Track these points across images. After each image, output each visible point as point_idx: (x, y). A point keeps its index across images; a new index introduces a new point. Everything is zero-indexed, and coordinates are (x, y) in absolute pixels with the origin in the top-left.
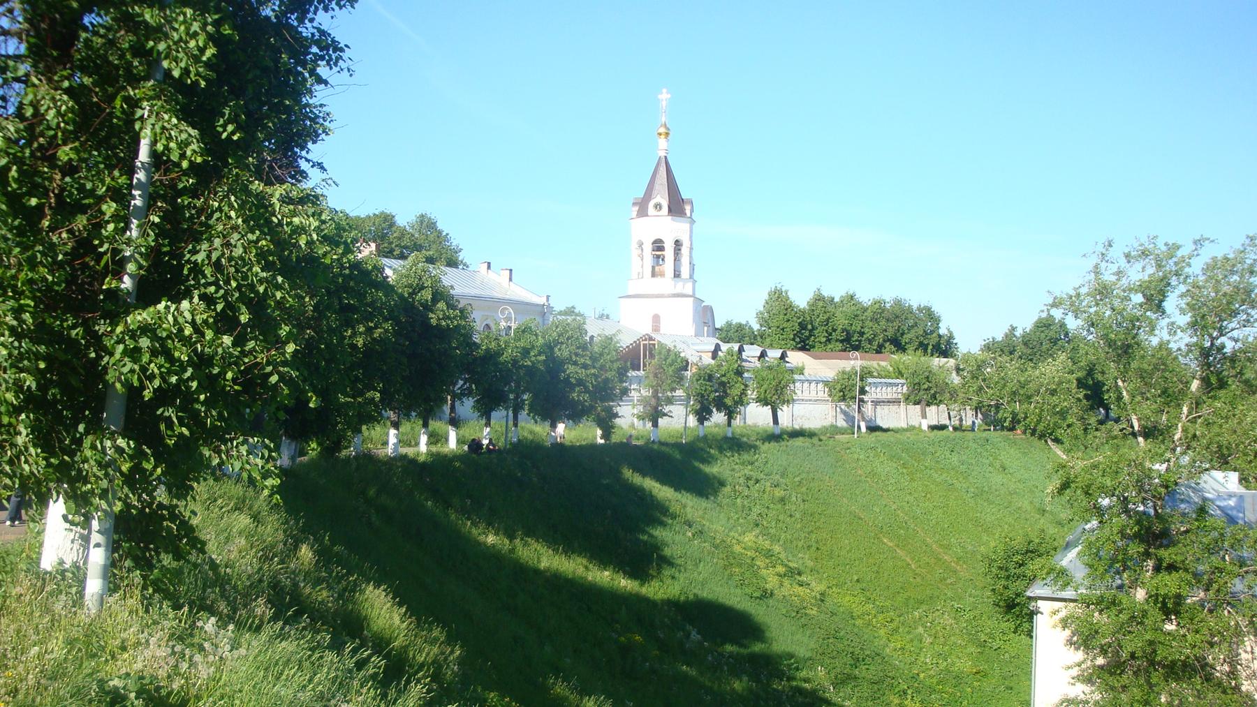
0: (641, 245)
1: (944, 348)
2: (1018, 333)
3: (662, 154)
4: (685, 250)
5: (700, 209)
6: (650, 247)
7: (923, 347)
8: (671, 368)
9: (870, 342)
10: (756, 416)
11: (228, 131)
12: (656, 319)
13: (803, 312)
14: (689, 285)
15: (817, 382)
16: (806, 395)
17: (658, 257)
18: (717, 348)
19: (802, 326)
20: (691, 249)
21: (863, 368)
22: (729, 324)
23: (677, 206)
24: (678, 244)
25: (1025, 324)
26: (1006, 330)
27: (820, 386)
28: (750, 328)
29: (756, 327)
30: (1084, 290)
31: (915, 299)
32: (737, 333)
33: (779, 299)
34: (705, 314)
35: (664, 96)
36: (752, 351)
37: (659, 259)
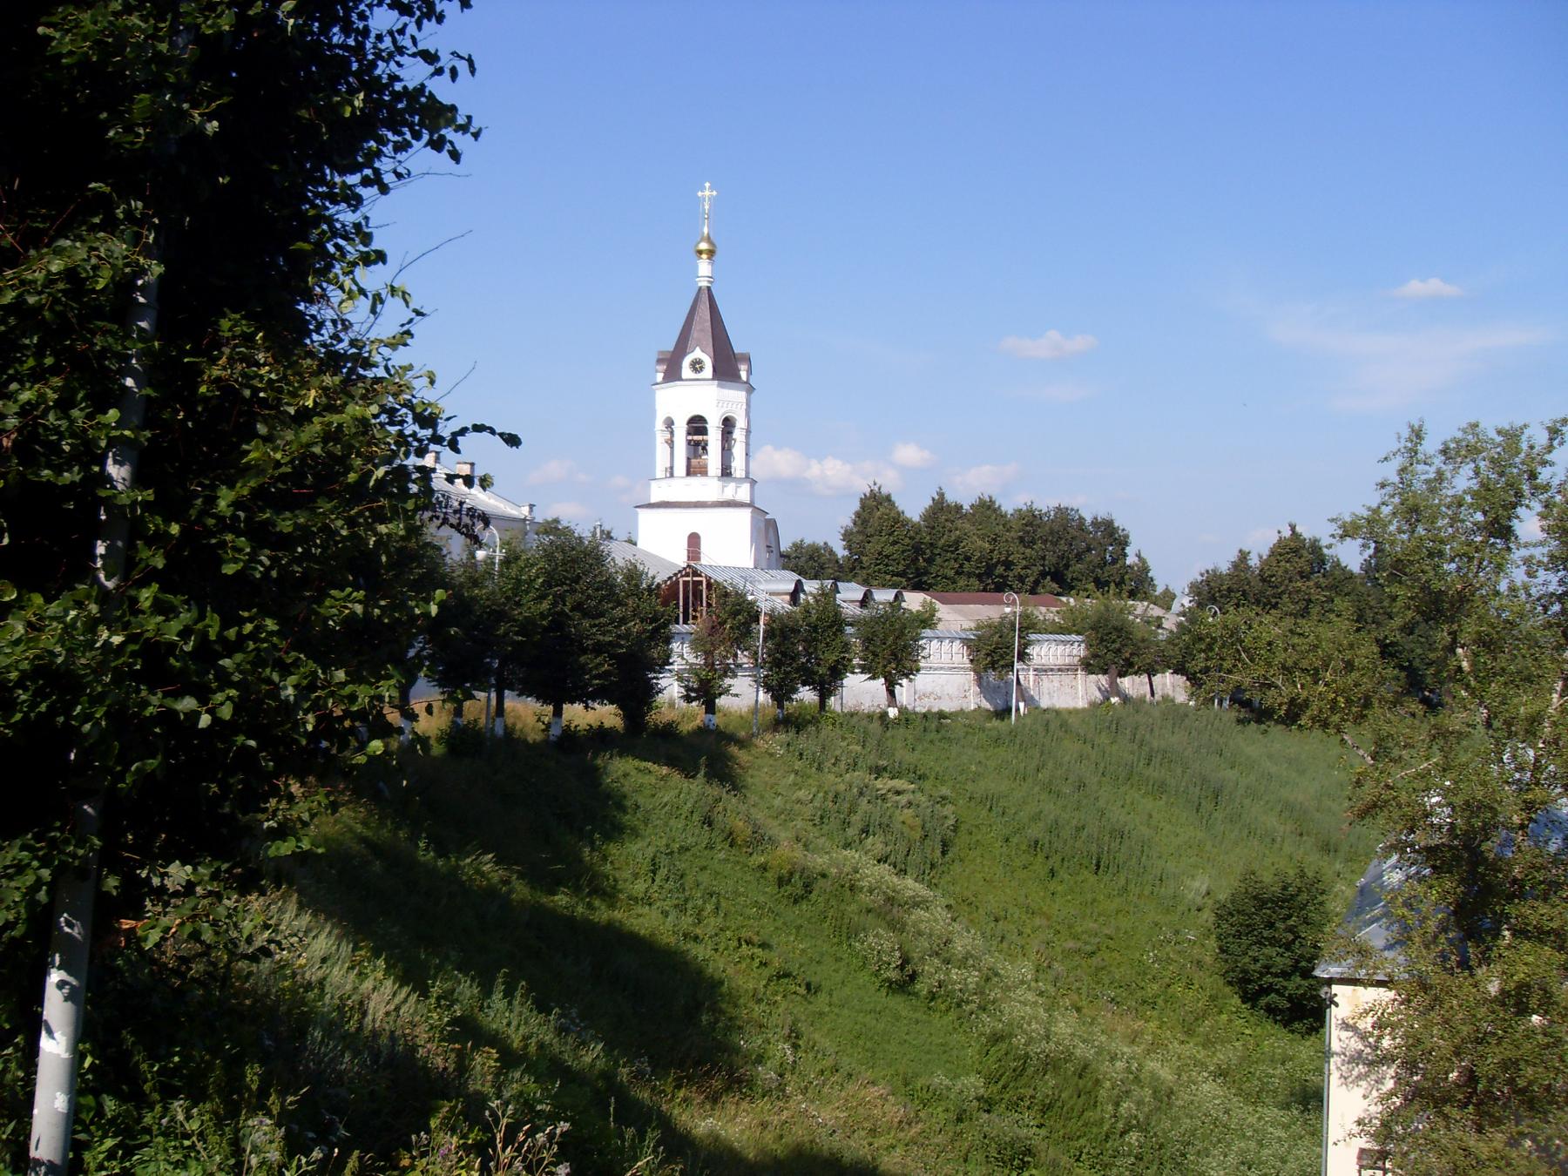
0: (669, 423)
1: (1138, 584)
2: (1254, 561)
3: (704, 283)
4: (739, 434)
5: (760, 372)
6: (685, 427)
7: (1100, 584)
8: (730, 615)
9: (1021, 579)
10: (860, 691)
11: (1114, 700)
12: (694, 540)
13: (917, 528)
14: (746, 487)
15: (952, 640)
16: (778, 599)
17: (697, 444)
18: (799, 587)
19: (917, 550)
20: (748, 432)
21: (1025, 616)
22: (797, 547)
23: (727, 367)
24: (728, 424)
25: (1260, 544)
26: (1233, 556)
27: (957, 644)
28: (832, 552)
29: (841, 551)
30: (1386, 510)
31: (1089, 508)
32: (807, 561)
33: (875, 508)
34: (766, 530)
35: (707, 193)
36: (849, 593)
37: (697, 448)
